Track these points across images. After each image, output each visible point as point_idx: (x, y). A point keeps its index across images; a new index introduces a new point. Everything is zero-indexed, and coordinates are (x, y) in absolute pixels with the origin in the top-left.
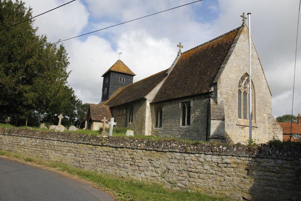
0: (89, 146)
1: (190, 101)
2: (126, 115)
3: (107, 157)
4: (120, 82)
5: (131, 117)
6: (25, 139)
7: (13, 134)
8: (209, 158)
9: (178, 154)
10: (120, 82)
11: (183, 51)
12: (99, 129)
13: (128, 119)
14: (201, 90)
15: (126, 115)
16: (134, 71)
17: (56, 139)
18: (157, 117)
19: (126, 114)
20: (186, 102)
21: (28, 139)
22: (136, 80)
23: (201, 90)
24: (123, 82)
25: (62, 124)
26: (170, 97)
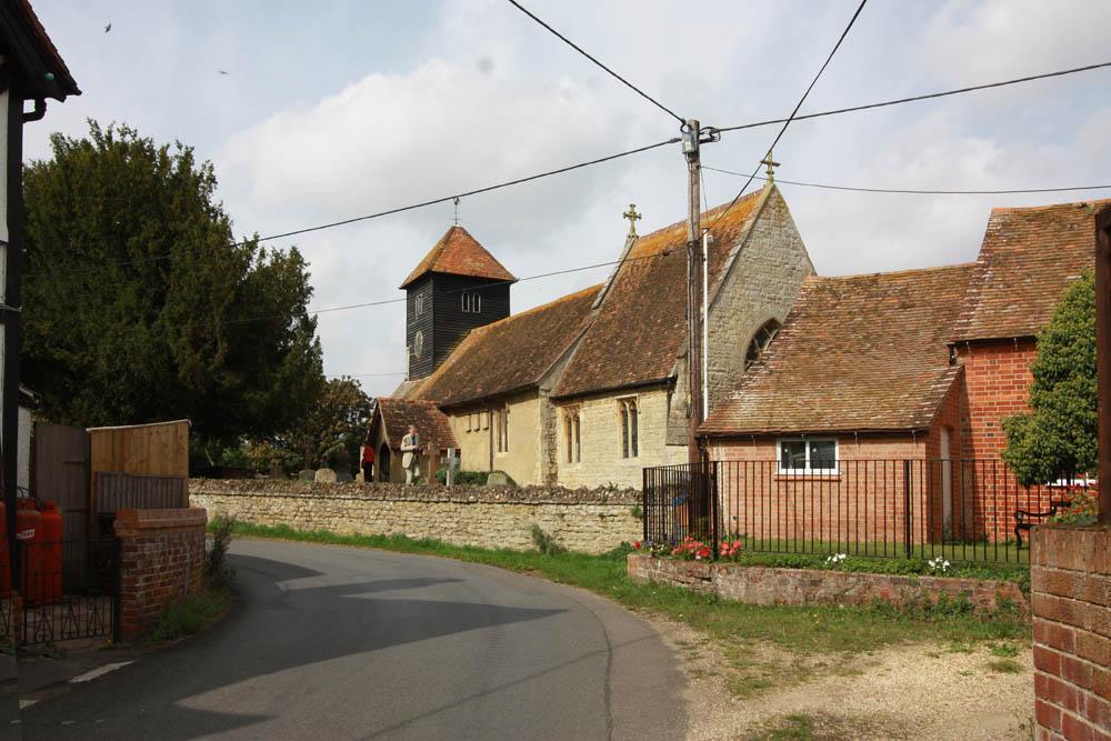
0: (415, 504)
1: (635, 398)
2: (488, 432)
3: (449, 520)
4: (466, 308)
5: (503, 437)
6: (280, 500)
7: (250, 493)
8: (591, 509)
9: (554, 507)
10: (466, 308)
11: (643, 229)
12: (273, 246)
13: (496, 441)
14: (654, 373)
15: (488, 432)
16: (509, 260)
17: (349, 497)
18: (570, 435)
19: (489, 428)
20: (628, 400)
21: (289, 500)
22: (522, 301)
23: (654, 373)
24: (477, 309)
25: (972, 591)
26: (595, 386)
